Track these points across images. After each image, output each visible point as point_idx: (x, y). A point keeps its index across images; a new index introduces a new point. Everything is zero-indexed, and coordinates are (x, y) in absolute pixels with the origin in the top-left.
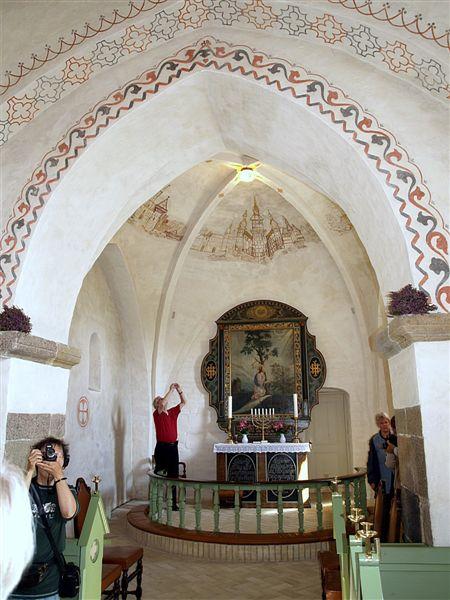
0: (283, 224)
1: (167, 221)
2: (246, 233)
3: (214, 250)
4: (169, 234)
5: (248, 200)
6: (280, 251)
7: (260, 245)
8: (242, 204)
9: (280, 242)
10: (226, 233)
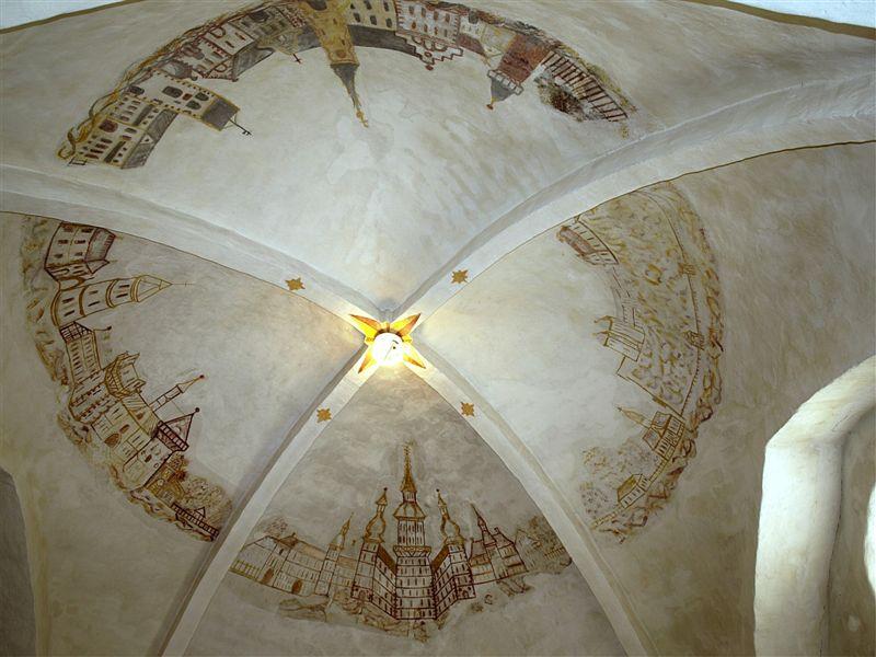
0: (472, 531)
1: (183, 476)
2: (381, 554)
3: (296, 587)
4: (182, 515)
5: (393, 457)
6: (463, 606)
7: (415, 588)
8: (377, 468)
9: (463, 580)
10: (333, 547)
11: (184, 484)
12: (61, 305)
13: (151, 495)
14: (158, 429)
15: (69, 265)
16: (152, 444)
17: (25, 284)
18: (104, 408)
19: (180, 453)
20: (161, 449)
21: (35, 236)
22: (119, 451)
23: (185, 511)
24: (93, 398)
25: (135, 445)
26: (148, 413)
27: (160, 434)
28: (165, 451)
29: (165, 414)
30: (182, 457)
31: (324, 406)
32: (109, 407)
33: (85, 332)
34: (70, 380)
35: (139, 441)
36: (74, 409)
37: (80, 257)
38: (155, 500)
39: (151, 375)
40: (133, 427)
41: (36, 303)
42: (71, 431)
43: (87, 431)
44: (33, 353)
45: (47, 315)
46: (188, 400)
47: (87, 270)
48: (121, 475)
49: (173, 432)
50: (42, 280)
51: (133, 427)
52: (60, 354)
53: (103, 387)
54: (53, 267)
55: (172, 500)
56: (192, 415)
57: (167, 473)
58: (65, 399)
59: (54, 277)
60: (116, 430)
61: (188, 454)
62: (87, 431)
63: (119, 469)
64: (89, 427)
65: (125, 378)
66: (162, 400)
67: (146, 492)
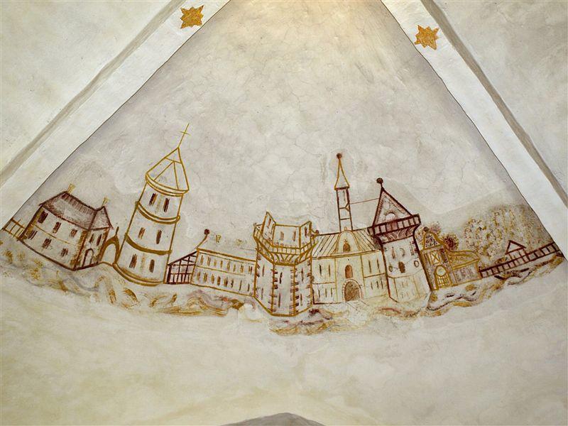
1: (451, 242)
4: (502, 271)
11: (462, 245)
12: (136, 271)
13: (449, 290)
14: (375, 236)
15: (83, 247)
16: (388, 254)
17: (81, 294)
18: (307, 280)
19: (420, 229)
20: (401, 247)
21: (25, 267)
22: (371, 292)
23: (499, 264)
24: (285, 286)
25: (375, 271)
26: (350, 238)
27: (383, 238)
28: (406, 244)
29: (363, 219)
30: (426, 229)
31: (412, 32)
32: (309, 275)
33: (192, 258)
34: (240, 299)
35: (374, 265)
36: (279, 311)
37: (79, 235)
38: (460, 290)
39: (304, 211)
40: (354, 262)
41: (112, 293)
42: (303, 328)
43: (317, 311)
44: (173, 320)
45: (136, 288)
46: (362, 186)
47: (103, 232)
48: (399, 307)
49: (391, 223)
50: (87, 278)
51: (354, 262)
52: (198, 295)
53: (279, 269)
54: (76, 262)
55: (474, 271)
56: (383, 190)
57: (434, 257)
58: (259, 314)
59: (91, 266)
60: (342, 281)
61: (426, 221)
62: (317, 311)
63: (390, 304)
64: (315, 307)
65: (287, 241)
66: (344, 213)
67: (441, 293)
